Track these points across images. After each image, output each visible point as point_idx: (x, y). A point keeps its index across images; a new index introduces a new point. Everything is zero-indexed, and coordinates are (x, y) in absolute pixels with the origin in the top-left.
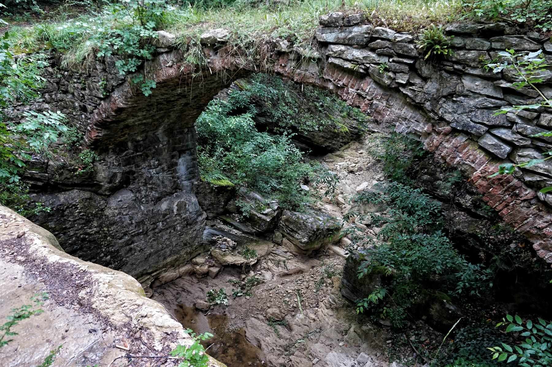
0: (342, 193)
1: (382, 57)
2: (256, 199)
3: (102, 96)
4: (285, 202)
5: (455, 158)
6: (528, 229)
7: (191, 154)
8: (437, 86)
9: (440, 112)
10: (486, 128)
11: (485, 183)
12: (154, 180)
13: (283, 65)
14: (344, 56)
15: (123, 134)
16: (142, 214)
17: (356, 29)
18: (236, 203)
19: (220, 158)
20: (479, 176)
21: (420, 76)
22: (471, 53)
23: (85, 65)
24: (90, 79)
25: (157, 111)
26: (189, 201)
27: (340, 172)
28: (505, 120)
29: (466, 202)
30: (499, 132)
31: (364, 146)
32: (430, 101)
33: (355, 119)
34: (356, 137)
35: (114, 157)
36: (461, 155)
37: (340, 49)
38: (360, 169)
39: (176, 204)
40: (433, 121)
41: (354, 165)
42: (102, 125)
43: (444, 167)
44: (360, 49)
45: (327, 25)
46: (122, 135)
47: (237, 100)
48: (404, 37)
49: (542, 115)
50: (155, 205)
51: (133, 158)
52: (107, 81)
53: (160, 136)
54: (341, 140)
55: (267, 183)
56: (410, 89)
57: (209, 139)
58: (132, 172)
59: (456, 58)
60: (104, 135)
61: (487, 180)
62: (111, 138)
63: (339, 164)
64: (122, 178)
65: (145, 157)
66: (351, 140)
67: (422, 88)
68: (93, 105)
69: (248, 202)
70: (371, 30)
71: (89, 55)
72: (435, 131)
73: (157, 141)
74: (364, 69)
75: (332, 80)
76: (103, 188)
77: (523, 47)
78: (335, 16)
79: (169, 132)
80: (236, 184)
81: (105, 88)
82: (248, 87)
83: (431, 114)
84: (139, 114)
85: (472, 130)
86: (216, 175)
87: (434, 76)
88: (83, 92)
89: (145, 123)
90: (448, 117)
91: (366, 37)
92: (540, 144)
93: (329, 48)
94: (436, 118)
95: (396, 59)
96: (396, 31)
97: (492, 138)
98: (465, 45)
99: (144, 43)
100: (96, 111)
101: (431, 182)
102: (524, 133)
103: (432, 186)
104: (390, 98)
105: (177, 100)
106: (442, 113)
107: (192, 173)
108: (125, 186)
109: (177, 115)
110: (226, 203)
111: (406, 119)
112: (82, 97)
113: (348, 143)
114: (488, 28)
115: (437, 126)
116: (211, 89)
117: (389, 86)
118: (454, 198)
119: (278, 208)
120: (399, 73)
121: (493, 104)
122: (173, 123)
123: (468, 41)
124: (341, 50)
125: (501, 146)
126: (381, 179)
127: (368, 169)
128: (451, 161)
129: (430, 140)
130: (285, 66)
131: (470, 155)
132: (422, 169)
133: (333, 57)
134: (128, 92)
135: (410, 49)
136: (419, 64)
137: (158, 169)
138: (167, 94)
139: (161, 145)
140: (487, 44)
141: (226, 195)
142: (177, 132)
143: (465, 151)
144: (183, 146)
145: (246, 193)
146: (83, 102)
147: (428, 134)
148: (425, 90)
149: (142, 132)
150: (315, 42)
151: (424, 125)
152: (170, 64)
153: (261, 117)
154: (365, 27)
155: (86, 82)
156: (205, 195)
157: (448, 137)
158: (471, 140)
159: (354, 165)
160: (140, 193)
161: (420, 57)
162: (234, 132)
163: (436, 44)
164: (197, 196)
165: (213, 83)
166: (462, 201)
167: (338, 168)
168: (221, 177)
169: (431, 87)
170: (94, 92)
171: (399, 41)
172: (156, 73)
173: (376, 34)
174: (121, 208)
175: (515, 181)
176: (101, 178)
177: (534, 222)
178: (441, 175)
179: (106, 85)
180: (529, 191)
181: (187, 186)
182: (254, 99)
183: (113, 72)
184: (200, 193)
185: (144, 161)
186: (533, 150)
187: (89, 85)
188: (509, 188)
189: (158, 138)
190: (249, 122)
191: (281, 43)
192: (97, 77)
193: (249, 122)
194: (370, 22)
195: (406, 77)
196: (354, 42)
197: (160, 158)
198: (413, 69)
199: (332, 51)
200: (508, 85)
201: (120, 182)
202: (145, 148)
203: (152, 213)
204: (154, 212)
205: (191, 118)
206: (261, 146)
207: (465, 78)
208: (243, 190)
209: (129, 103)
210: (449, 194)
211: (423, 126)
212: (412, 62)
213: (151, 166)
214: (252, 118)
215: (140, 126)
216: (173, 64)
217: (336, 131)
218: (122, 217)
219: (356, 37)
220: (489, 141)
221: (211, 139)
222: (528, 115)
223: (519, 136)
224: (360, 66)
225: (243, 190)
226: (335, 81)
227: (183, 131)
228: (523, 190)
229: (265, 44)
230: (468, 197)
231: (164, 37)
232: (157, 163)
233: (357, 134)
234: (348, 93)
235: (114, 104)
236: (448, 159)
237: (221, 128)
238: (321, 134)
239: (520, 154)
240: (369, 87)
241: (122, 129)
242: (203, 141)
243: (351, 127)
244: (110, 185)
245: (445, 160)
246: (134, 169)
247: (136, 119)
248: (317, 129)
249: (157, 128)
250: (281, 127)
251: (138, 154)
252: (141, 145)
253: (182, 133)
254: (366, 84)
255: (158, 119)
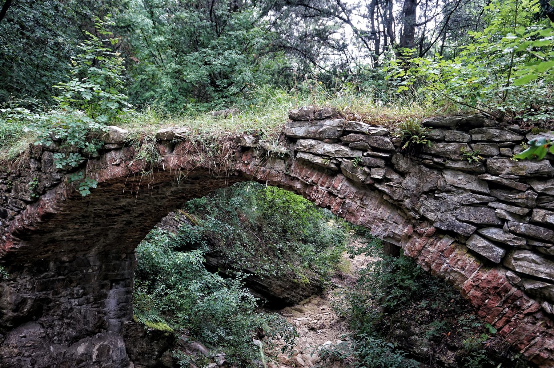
0: (301, 353)
1: (355, 151)
2: (198, 350)
3: (29, 199)
4: (234, 355)
5: (441, 264)
6: (537, 352)
7: (126, 286)
8: (416, 180)
9: (421, 211)
10: (474, 228)
11: (478, 294)
12: (74, 313)
13: (246, 162)
14: (314, 151)
15: (46, 249)
16: (50, 357)
17: (328, 122)
18: (173, 355)
19: (159, 296)
20: (471, 285)
21: (397, 172)
22: (451, 145)
23: (17, 164)
24: (19, 179)
25: (93, 226)
26: (114, 346)
27: (300, 328)
28: (494, 218)
29: (449, 359)
30: (489, 232)
31: (326, 302)
32: (409, 197)
33: (316, 272)
34: (317, 291)
35: (28, 279)
36: (448, 261)
37: (309, 143)
38: (322, 326)
39: (97, 347)
40: (413, 221)
41: (315, 321)
42: (22, 234)
43: (418, 320)
44: (331, 144)
45: (295, 119)
46: (44, 251)
47: (188, 234)
48: (379, 129)
49: (534, 210)
50: (69, 346)
51: (53, 282)
52: (40, 181)
53: (91, 259)
54: (301, 293)
55: (213, 331)
56: (387, 185)
57: (150, 275)
58: (47, 300)
59: (436, 151)
60: (22, 248)
61: (481, 290)
62: (30, 253)
63: (299, 319)
64: (32, 306)
65: (68, 283)
66: (313, 294)
67: (401, 183)
68: (16, 209)
69: (188, 354)
70: (343, 123)
71: (23, 153)
72: (417, 232)
73: (87, 264)
74: (335, 164)
75: (300, 178)
76: (5, 318)
77: (504, 138)
78: (305, 109)
79: (104, 255)
80: (175, 330)
81: (35, 190)
82: (202, 222)
83: (412, 213)
84: (71, 226)
85: (459, 229)
86: (152, 316)
87: (413, 170)
88: (7, 195)
89: (75, 240)
90: (430, 216)
91: (338, 131)
92: (536, 244)
93: (298, 143)
94: (417, 217)
95: (370, 152)
96: (370, 124)
97: (482, 239)
98: (444, 137)
99: (90, 136)
100: (18, 217)
101: (405, 337)
102: (518, 232)
103: (407, 342)
104: (365, 197)
105: (118, 215)
106: (423, 211)
107: (124, 310)
108: (34, 317)
109: (116, 235)
110: (161, 353)
111: (383, 220)
112: (4, 200)
113: (309, 296)
114: (466, 120)
115: (419, 227)
116: (160, 206)
117: (363, 182)
118: (434, 355)
119: (225, 363)
120: (374, 167)
121: (479, 199)
122: (110, 245)
123: (447, 133)
124: (311, 145)
125: (492, 248)
126: (347, 339)
127: (332, 327)
128: (437, 268)
129: (412, 244)
130: (249, 164)
131: (459, 260)
132: (394, 322)
133: (302, 152)
134: (62, 194)
135: (385, 142)
136: (396, 158)
137: (82, 299)
138: (108, 204)
139: (90, 271)
140: (467, 136)
141: (162, 342)
142: (113, 257)
143: (452, 255)
144: (117, 275)
145: (187, 342)
146: (5, 207)
147: (409, 237)
148: (403, 186)
149: (71, 251)
150: (283, 138)
151: (403, 227)
152: (118, 162)
153: (213, 257)
154: (337, 120)
155: (14, 183)
156: (136, 340)
157: (432, 240)
158: (458, 242)
159: (315, 321)
160: (52, 329)
161: (396, 150)
162: (179, 269)
163: (413, 135)
164: (125, 341)
165: (163, 198)
166: (443, 359)
167: (298, 324)
168: (158, 318)
169: (410, 182)
170: (20, 194)
171: (373, 134)
172: (99, 172)
173: (349, 127)
174: (23, 346)
175: (514, 290)
176: (5, 303)
177: (544, 343)
178: (416, 329)
179: (37, 185)
180: (531, 302)
181: (115, 326)
182: (206, 236)
183: (48, 171)
184: (130, 337)
185: (66, 287)
186: (530, 252)
187: (16, 186)
188: (508, 298)
189: (88, 262)
190: (198, 259)
191: (246, 138)
192: (28, 177)
193: (198, 259)
194: (342, 116)
195: (383, 172)
196: (326, 135)
197: (87, 286)
198: (389, 165)
199: (302, 145)
200: (495, 178)
201: (28, 311)
202: (70, 271)
203: (64, 358)
204: (66, 356)
205: (133, 242)
206: (210, 285)
207: (446, 172)
208: (184, 338)
209: (61, 209)
210: (427, 351)
211: (402, 229)
212: (388, 155)
213: (73, 295)
214: (203, 255)
215: (69, 243)
216: (121, 163)
217: (296, 281)
218: (22, 359)
219: (328, 131)
220: (478, 243)
221: (152, 275)
222: (519, 211)
223: (512, 236)
224: (332, 161)
225: (184, 338)
226: (302, 178)
227: (120, 257)
228: (524, 301)
229: (228, 141)
230: (450, 353)
231: (116, 131)
232: (81, 291)
233: (318, 287)
234: (317, 192)
235: (42, 208)
236: (433, 266)
237: (165, 262)
238: (279, 283)
239: (515, 256)
240: (341, 185)
241: (46, 243)
242: (143, 276)
243: (312, 279)
244: (15, 314)
245: (430, 268)
246: (51, 296)
247: (66, 232)
248: (275, 274)
249: (89, 249)
250: (234, 269)
251: (60, 277)
252: (65, 268)
253: (118, 258)
254: (338, 181)
255: (92, 237)
